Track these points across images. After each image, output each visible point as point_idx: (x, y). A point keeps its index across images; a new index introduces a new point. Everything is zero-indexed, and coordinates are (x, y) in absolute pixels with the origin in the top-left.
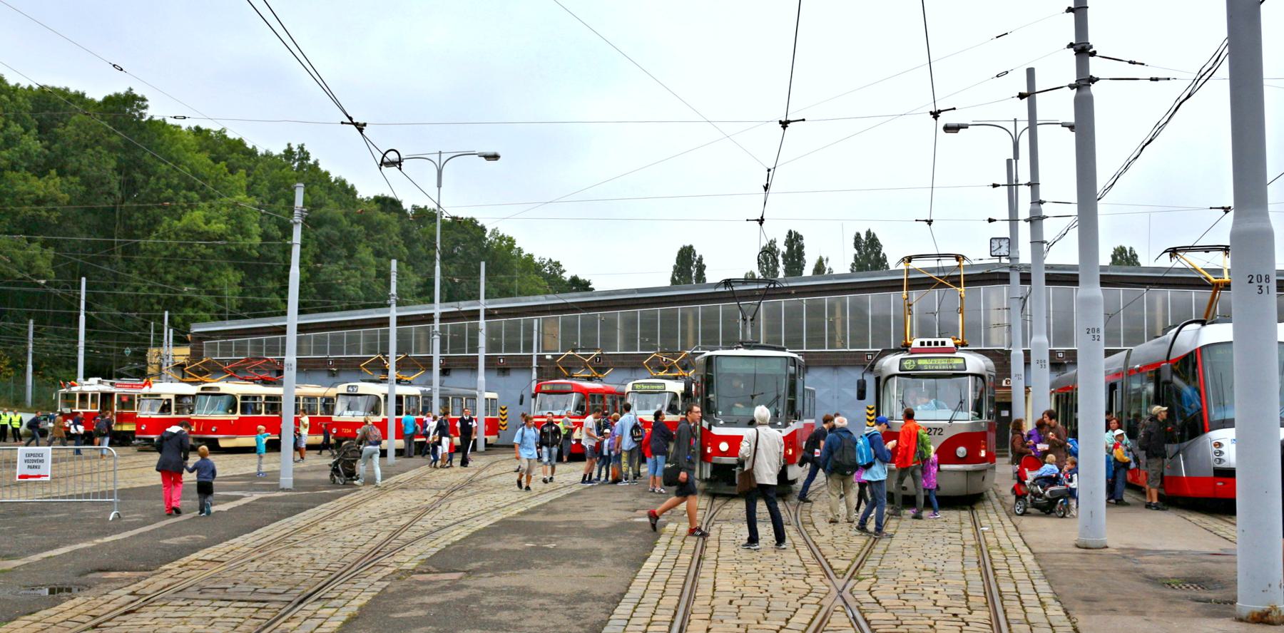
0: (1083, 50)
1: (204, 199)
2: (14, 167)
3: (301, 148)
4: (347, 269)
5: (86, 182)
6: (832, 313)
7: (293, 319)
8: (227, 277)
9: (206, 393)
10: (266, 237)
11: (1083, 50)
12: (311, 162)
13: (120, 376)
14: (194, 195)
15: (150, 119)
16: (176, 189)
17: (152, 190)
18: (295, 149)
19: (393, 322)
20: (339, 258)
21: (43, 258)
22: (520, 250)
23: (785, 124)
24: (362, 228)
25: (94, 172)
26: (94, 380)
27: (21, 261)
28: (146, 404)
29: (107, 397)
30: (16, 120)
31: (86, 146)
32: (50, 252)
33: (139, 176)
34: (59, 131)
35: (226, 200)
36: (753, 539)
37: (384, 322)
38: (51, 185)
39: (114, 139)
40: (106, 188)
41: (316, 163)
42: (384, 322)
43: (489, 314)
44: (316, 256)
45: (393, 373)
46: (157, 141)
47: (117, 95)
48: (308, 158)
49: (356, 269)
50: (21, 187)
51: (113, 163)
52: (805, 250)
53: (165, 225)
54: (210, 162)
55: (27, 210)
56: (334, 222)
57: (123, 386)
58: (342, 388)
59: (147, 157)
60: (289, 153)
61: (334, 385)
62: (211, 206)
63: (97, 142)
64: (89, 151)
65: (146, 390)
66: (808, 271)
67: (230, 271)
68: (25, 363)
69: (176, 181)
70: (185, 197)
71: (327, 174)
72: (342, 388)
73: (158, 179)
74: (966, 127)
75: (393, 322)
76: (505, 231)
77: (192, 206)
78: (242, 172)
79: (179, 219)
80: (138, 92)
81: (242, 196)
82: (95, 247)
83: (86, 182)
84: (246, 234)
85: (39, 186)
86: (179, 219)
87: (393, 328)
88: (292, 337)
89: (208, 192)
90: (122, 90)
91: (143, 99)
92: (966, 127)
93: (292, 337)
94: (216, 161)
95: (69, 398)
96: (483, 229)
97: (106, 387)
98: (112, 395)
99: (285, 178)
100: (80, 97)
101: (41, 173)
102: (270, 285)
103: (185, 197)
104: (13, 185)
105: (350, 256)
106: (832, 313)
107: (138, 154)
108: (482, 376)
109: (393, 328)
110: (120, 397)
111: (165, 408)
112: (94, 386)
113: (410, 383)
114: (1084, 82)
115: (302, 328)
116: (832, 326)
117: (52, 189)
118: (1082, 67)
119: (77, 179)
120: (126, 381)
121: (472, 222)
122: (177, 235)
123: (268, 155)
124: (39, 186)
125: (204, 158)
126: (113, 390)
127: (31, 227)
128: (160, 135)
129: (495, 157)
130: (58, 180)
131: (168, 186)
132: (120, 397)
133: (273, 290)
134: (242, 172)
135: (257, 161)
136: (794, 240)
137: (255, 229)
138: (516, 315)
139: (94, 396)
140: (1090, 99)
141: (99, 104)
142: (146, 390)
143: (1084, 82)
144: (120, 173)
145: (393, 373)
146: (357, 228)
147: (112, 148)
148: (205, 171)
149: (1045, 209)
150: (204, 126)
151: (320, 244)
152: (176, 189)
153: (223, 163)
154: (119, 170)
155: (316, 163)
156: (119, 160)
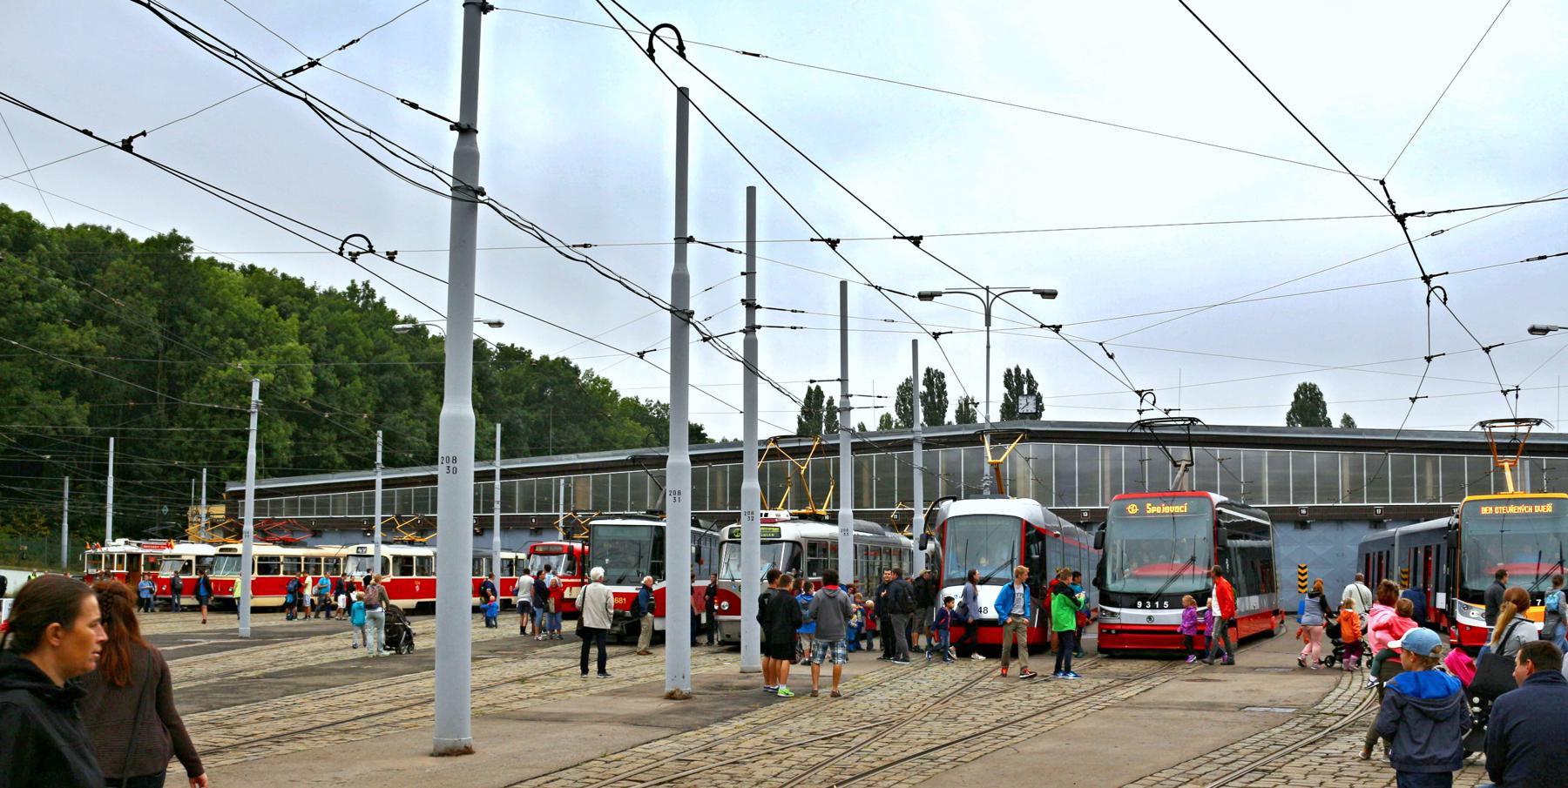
0: (750, 305)
1: (252, 346)
2: (50, 318)
3: (366, 285)
4: (411, 417)
5: (126, 331)
6: (713, 480)
7: (250, 485)
8: (277, 431)
9: (224, 554)
10: (321, 387)
11: (750, 305)
12: (377, 300)
13: (147, 537)
14: (242, 343)
15: (198, 259)
16: (222, 336)
17: (197, 338)
18: (360, 286)
19: (379, 485)
20: (404, 407)
21: (77, 415)
22: (616, 394)
23: (1429, 359)
24: (429, 372)
25: (133, 321)
26: (121, 541)
27: (55, 418)
28: (167, 564)
29: (134, 558)
30: (51, 267)
31: (126, 293)
32: (86, 408)
33: (182, 323)
34: (98, 277)
35: (275, 347)
36: (585, 670)
37: (371, 485)
38: (86, 336)
39: (156, 285)
40: (146, 337)
41: (382, 301)
42: (371, 485)
43: (506, 474)
44: (378, 404)
45: (378, 535)
46: (202, 285)
47: (160, 237)
48: (373, 296)
49: (423, 419)
50: (55, 339)
51: (154, 310)
52: (947, 389)
53: (209, 375)
54: (260, 306)
55: (62, 362)
56: (398, 369)
57: (150, 547)
58: (352, 550)
59: (191, 302)
60: (353, 289)
61: (347, 545)
62: (260, 354)
63: (139, 288)
64: (129, 297)
65: (167, 551)
66: (950, 416)
67: (281, 422)
68: (61, 522)
69: (222, 329)
70: (232, 345)
71: (394, 312)
72: (352, 550)
73: (202, 328)
74: (939, 294)
75: (379, 485)
76: (601, 373)
77: (238, 354)
78: (295, 316)
79: (225, 369)
80: (182, 233)
81: (293, 344)
82: (138, 397)
83: (126, 331)
84: (297, 384)
85: (73, 337)
86: (225, 369)
87: (379, 490)
88: (250, 502)
89: (258, 339)
90: (166, 232)
91: (188, 241)
92: (939, 294)
93: (250, 502)
94: (266, 304)
95: (96, 559)
96: (576, 371)
97: (133, 549)
98: (139, 555)
99: (346, 321)
100: (121, 237)
101: (77, 322)
102: (326, 436)
103: (232, 345)
104: (47, 335)
105: (416, 404)
106: (713, 480)
107: (181, 299)
108: (497, 538)
109: (379, 490)
110: (147, 557)
111: (187, 568)
112: (119, 546)
113: (424, 544)
114: (751, 329)
115: (259, 493)
116: (713, 492)
117: (88, 341)
118: (750, 316)
119: (116, 329)
120: (153, 542)
121: (563, 363)
122: (222, 385)
123: (331, 293)
124: (73, 337)
125: (253, 302)
126: (139, 550)
127: (66, 382)
128: (205, 279)
129: (499, 324)
130: (94, 331)
131: (214, 333)
132: (147, 557)
133: (330, 441)
134: (295, 316)
135: (315, 304)
136: (935, 381)
137: (308, 378)
138: (548, 474)
139: (121, 557)
140: (756, 341)
141: (142, 245)
142: (167, 551)
143: (751, 329)
144: (161, 321)
145: (378, 535)
146: (422, 374)
147: (154, 294)
148: (255, 316)
149: (853, 402)
150: (259, 265)
151: (383, 392)
152: (222, 336)
153: (273, 307)
154: (160, 318)
155: (382, 301)
156: (159, 306)
